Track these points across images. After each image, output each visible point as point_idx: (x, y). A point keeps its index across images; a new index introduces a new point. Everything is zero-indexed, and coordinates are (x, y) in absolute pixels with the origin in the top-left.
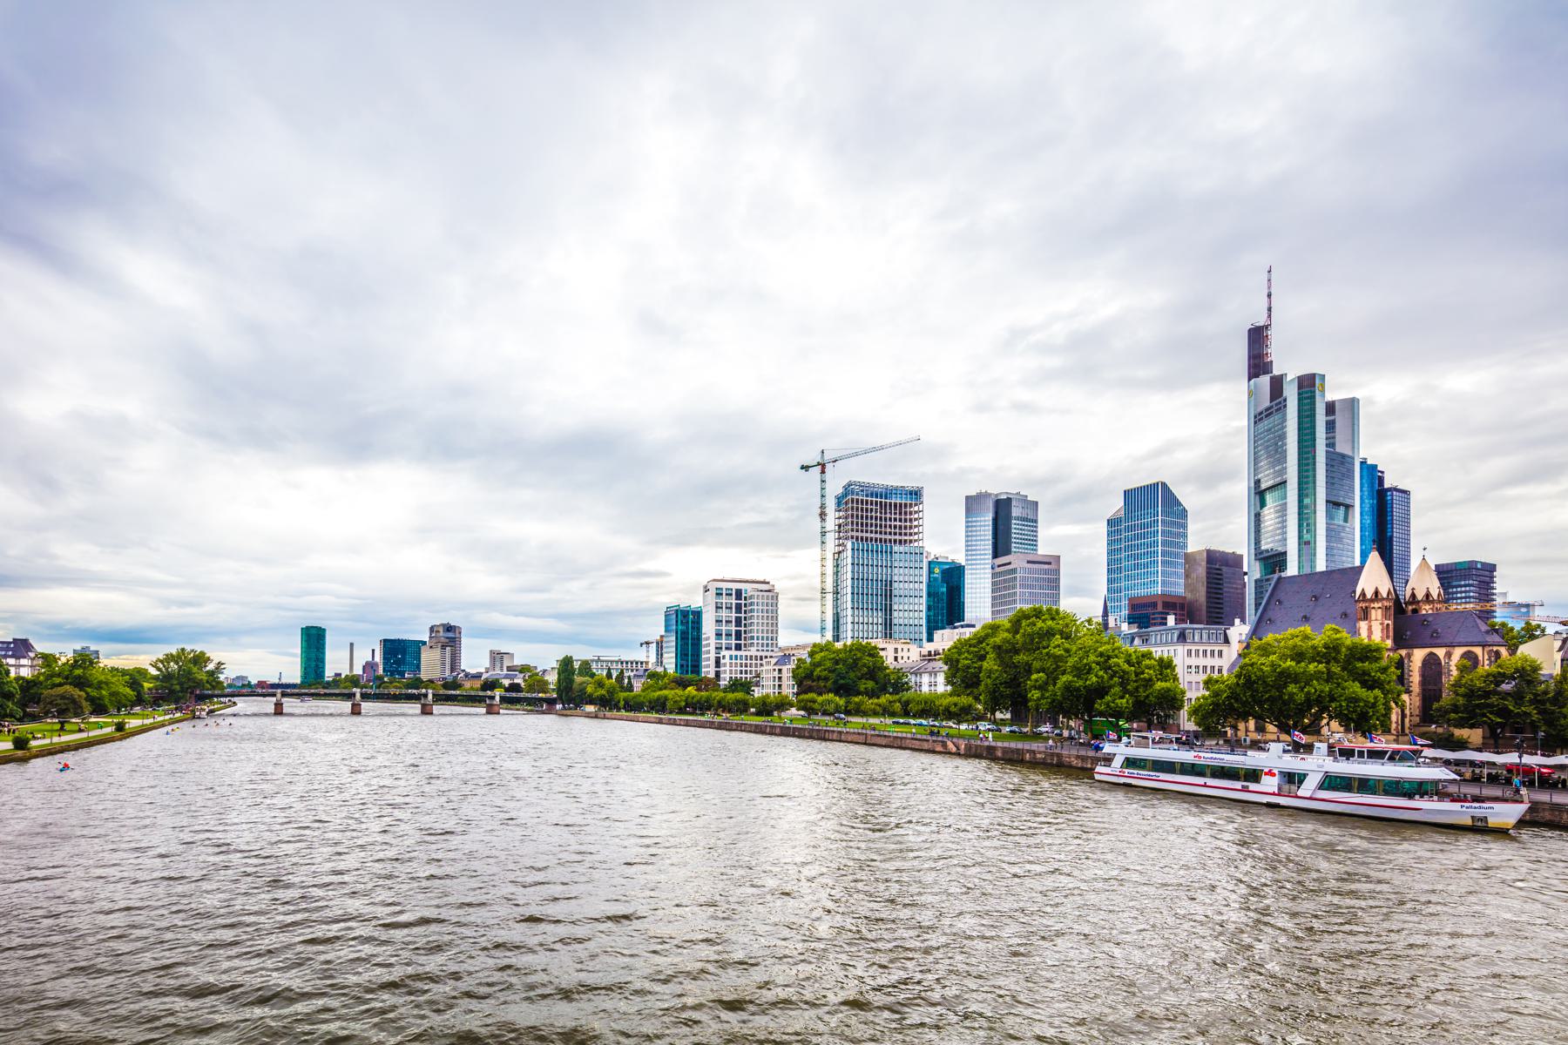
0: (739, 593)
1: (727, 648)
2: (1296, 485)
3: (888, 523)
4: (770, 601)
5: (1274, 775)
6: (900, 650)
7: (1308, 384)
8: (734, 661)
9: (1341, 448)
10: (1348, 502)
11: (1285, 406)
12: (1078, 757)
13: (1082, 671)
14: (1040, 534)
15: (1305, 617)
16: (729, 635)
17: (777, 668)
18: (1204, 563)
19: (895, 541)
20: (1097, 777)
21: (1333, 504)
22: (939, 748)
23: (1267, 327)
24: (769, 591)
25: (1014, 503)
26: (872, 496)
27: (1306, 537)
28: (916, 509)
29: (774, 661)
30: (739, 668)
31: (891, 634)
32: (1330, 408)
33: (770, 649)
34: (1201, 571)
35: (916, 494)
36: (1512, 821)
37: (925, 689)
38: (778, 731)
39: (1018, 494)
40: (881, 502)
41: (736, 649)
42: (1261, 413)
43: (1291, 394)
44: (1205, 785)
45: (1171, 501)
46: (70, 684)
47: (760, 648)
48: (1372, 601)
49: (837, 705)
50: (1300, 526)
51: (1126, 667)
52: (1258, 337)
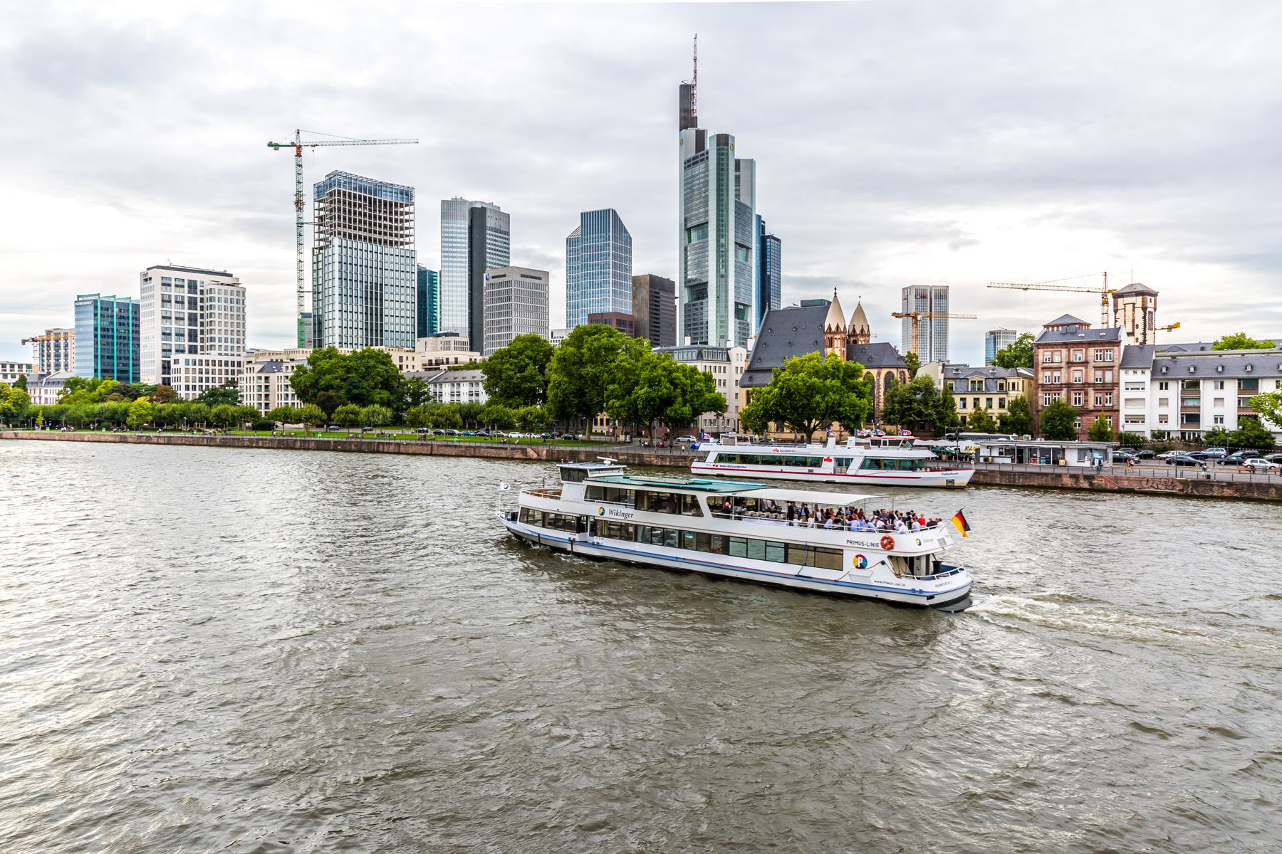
0: (193, 286)
1: (177, 351)
2: (715, 227)
4: (235, 297)
5: (830, 460)
6: (404, 359)
7: (724, 141)
9: (744, 200)
10: (748, 245)
12: (657, 457)
13: (651, 382)
14: (512, 247)
17: (263, 375)
18: (647, 287)
20: (693, 471)
21: (739, 245)
22: (518, 455)
23: (693, 86)
24: (233, 285)
25: (488, 214)
27: (723, 271)
28: (406, 209)
29: (258, 367)
30: (198, 375)
31: (382, 340)
32: (738, 162)
34: (645, 294)
35: (407, 194)
36: (967, 481)
37: (446, 399)
38: (312, 445)
39: (491, 204)
40: (370, 198)
41: (190, 352)
42: (689, 161)
43: (711, 146)
44: (782, 472)
45: (620, 228)
47: (223, 352)
48: (835, 333)
49: (384, 416)
50: (718, 261)
51: (683, 379)
52: (687, 92)
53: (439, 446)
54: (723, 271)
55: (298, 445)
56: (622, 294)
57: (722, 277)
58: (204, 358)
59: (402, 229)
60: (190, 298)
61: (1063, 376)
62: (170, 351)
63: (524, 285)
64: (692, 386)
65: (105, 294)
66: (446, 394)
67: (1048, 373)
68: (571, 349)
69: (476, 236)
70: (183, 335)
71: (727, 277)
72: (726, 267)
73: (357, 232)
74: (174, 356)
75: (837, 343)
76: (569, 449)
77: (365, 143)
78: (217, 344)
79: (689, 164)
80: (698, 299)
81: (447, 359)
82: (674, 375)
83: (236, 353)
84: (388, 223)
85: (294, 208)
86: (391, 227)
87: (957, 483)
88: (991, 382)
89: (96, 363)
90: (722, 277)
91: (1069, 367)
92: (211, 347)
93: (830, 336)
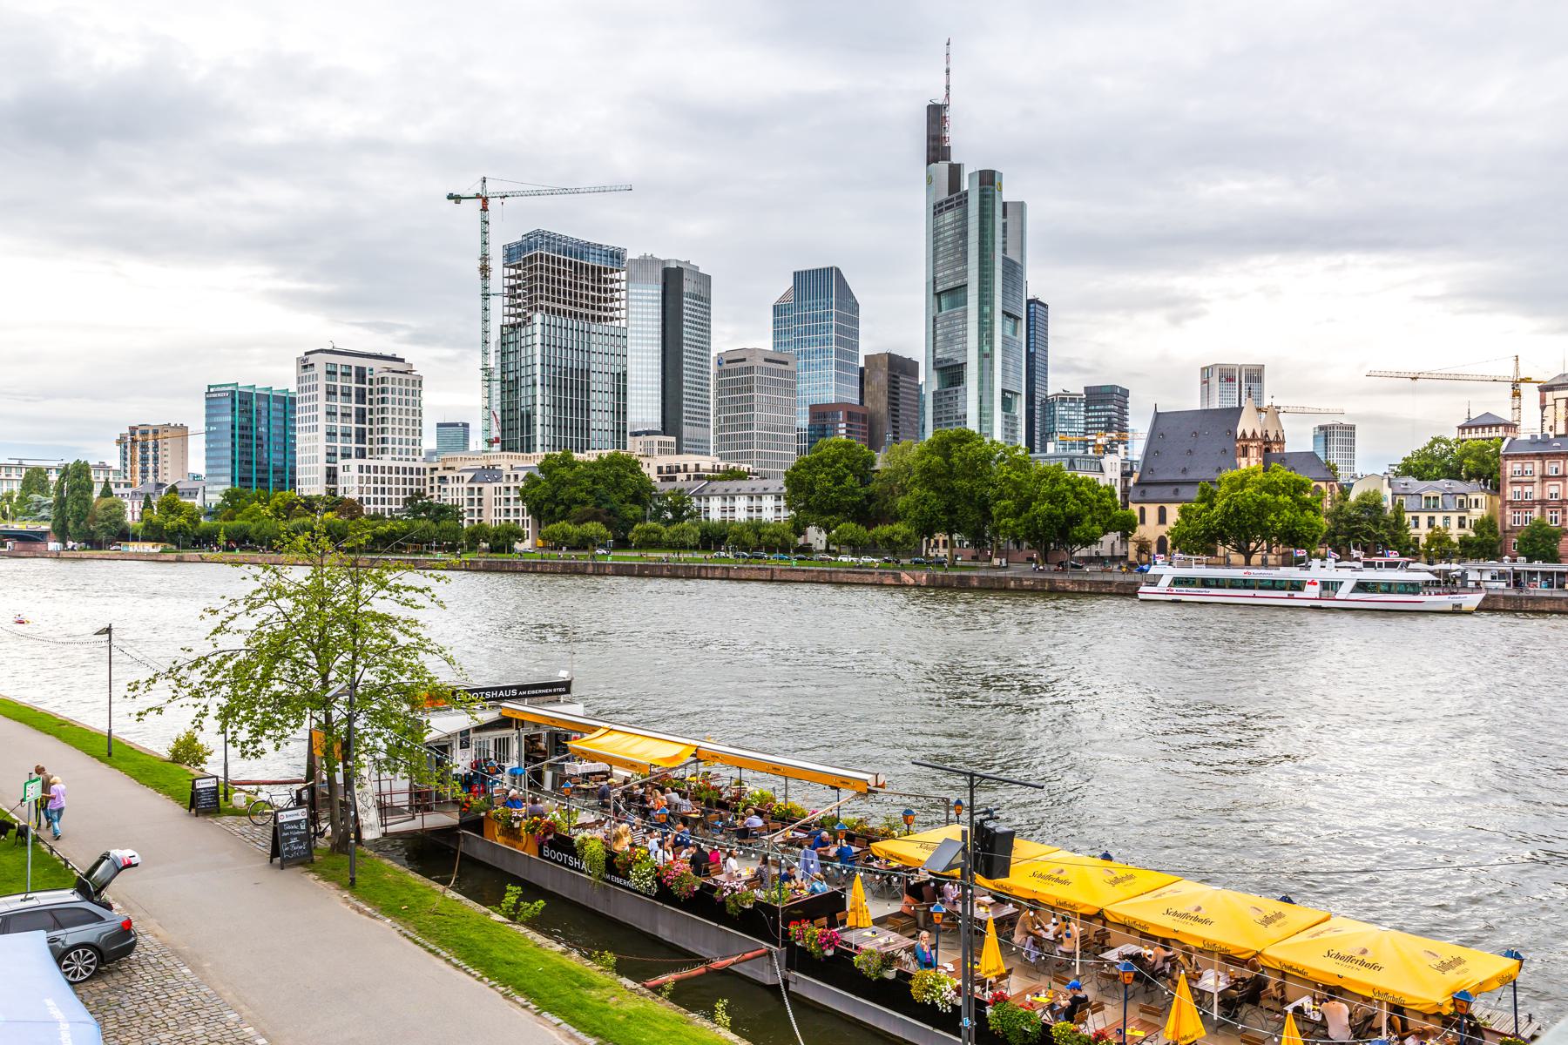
0: (361, 374)
2: (976, 291)
3: (584, 292)
5: (1315, 584)
7: (988, 179)
8: (365, 475)
9: (1013, 255)
10: (1017, 314)
11: (966, 201)
12: (1073, 582)
13: (1053, 498)
15: (1190, 451)
16: (346, 435)
17: (476, 486)
18: (885, 369)
19: (593, 317)
22: (890, 581)
25: (685, 275)
26: (559, 253)
29: (468, 476)
32: (1005, 205)
33: (411, 457)
39: (688, 262)
40: (576, 263)
42: (941, 204)
44: (1254, 596)
46: (430, 518)
47: (397, 456)
48: (1251, 440)
52: (936, 115)
53: (781, 570)
54: (987, 349)
55: (590, 569)
56: (846, 377)
57: (985, 357)
58: (373, 463)
59: (612, 300)
60: (357, 389)
61: (1536, 492)
62: (335, 454)
63: (769, 371)
64: (1099, 501)
65: (244, 383)
66: (715, 510)
67: (1517, 488)
68: (937, 458)
69: (670, 305)
70: (350, 435)
71: (993, 356)
72: (991, 343)
73: (562, 307)
74: (341, 463)
75: (1253, 452)
76: (958, 574)
77: (565, 191)
78: (390, 446)
79: (938, 209)
80: (952, 384)
81: (685, 466)
82: (1079, 489)
83: (411, 457)
84: (596, 294)
85: (478, 275)
86: (599, 299)
87: (1464, 608)
88: (1448, 499)
89: (233, 469)
90: (985, 357)
91: (1543, 481)
92: (383, 451)
93: (1244, 443)
